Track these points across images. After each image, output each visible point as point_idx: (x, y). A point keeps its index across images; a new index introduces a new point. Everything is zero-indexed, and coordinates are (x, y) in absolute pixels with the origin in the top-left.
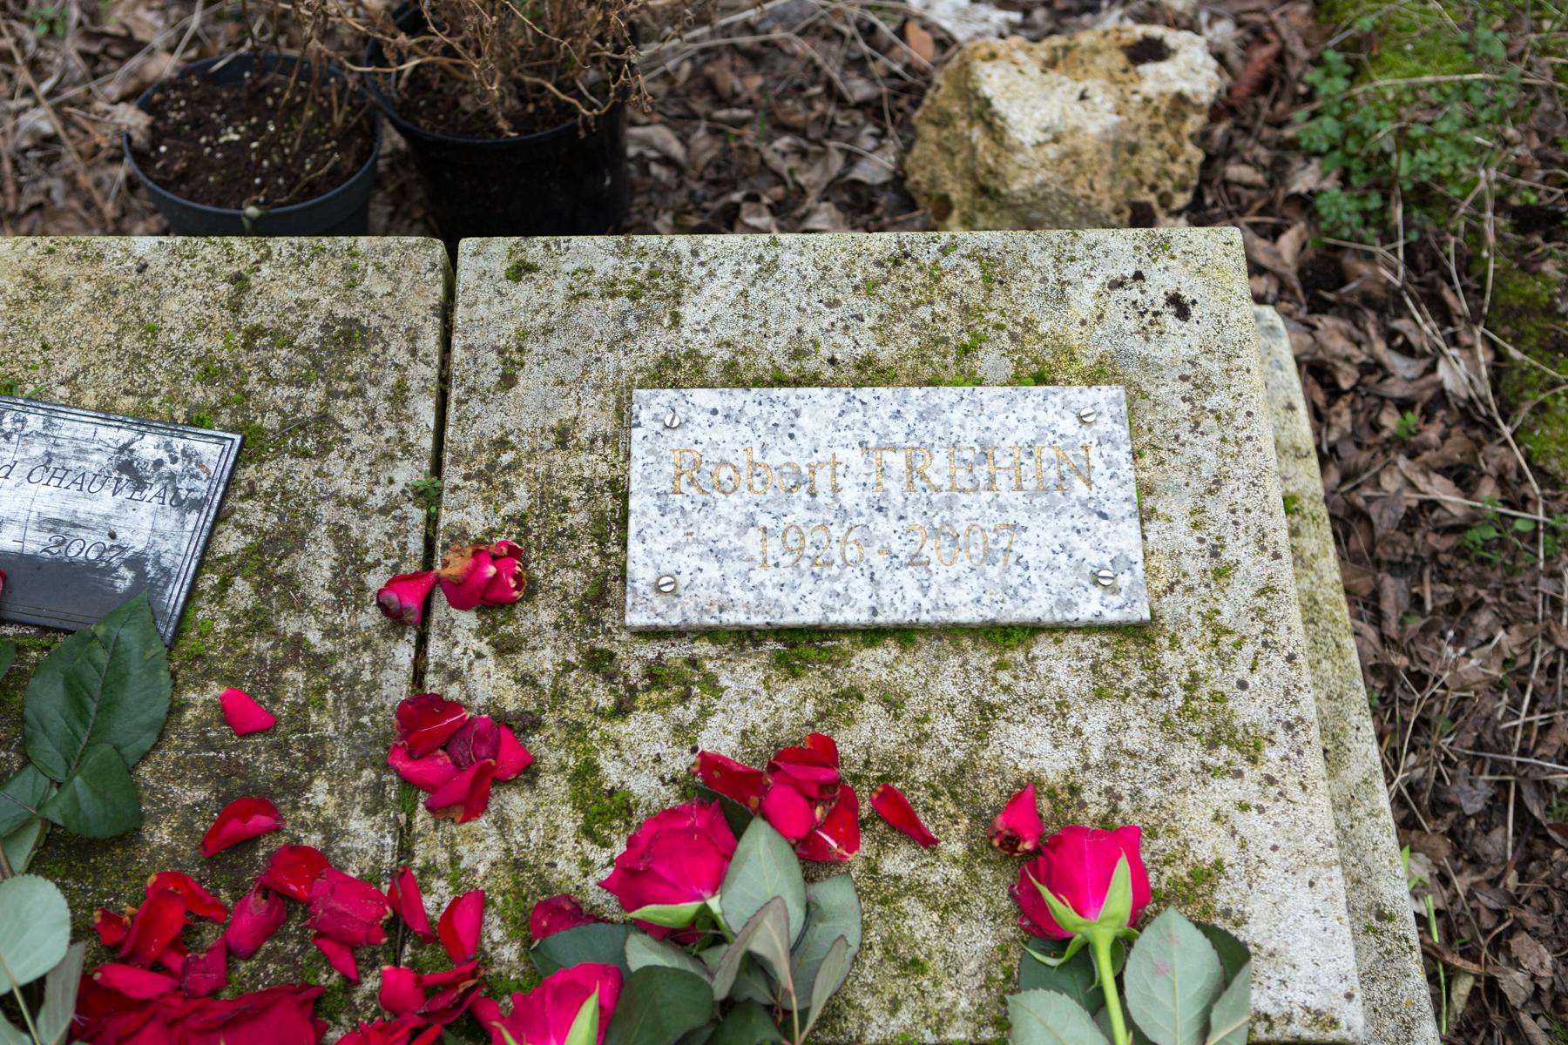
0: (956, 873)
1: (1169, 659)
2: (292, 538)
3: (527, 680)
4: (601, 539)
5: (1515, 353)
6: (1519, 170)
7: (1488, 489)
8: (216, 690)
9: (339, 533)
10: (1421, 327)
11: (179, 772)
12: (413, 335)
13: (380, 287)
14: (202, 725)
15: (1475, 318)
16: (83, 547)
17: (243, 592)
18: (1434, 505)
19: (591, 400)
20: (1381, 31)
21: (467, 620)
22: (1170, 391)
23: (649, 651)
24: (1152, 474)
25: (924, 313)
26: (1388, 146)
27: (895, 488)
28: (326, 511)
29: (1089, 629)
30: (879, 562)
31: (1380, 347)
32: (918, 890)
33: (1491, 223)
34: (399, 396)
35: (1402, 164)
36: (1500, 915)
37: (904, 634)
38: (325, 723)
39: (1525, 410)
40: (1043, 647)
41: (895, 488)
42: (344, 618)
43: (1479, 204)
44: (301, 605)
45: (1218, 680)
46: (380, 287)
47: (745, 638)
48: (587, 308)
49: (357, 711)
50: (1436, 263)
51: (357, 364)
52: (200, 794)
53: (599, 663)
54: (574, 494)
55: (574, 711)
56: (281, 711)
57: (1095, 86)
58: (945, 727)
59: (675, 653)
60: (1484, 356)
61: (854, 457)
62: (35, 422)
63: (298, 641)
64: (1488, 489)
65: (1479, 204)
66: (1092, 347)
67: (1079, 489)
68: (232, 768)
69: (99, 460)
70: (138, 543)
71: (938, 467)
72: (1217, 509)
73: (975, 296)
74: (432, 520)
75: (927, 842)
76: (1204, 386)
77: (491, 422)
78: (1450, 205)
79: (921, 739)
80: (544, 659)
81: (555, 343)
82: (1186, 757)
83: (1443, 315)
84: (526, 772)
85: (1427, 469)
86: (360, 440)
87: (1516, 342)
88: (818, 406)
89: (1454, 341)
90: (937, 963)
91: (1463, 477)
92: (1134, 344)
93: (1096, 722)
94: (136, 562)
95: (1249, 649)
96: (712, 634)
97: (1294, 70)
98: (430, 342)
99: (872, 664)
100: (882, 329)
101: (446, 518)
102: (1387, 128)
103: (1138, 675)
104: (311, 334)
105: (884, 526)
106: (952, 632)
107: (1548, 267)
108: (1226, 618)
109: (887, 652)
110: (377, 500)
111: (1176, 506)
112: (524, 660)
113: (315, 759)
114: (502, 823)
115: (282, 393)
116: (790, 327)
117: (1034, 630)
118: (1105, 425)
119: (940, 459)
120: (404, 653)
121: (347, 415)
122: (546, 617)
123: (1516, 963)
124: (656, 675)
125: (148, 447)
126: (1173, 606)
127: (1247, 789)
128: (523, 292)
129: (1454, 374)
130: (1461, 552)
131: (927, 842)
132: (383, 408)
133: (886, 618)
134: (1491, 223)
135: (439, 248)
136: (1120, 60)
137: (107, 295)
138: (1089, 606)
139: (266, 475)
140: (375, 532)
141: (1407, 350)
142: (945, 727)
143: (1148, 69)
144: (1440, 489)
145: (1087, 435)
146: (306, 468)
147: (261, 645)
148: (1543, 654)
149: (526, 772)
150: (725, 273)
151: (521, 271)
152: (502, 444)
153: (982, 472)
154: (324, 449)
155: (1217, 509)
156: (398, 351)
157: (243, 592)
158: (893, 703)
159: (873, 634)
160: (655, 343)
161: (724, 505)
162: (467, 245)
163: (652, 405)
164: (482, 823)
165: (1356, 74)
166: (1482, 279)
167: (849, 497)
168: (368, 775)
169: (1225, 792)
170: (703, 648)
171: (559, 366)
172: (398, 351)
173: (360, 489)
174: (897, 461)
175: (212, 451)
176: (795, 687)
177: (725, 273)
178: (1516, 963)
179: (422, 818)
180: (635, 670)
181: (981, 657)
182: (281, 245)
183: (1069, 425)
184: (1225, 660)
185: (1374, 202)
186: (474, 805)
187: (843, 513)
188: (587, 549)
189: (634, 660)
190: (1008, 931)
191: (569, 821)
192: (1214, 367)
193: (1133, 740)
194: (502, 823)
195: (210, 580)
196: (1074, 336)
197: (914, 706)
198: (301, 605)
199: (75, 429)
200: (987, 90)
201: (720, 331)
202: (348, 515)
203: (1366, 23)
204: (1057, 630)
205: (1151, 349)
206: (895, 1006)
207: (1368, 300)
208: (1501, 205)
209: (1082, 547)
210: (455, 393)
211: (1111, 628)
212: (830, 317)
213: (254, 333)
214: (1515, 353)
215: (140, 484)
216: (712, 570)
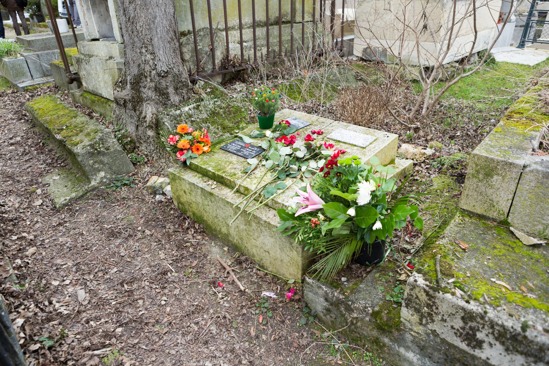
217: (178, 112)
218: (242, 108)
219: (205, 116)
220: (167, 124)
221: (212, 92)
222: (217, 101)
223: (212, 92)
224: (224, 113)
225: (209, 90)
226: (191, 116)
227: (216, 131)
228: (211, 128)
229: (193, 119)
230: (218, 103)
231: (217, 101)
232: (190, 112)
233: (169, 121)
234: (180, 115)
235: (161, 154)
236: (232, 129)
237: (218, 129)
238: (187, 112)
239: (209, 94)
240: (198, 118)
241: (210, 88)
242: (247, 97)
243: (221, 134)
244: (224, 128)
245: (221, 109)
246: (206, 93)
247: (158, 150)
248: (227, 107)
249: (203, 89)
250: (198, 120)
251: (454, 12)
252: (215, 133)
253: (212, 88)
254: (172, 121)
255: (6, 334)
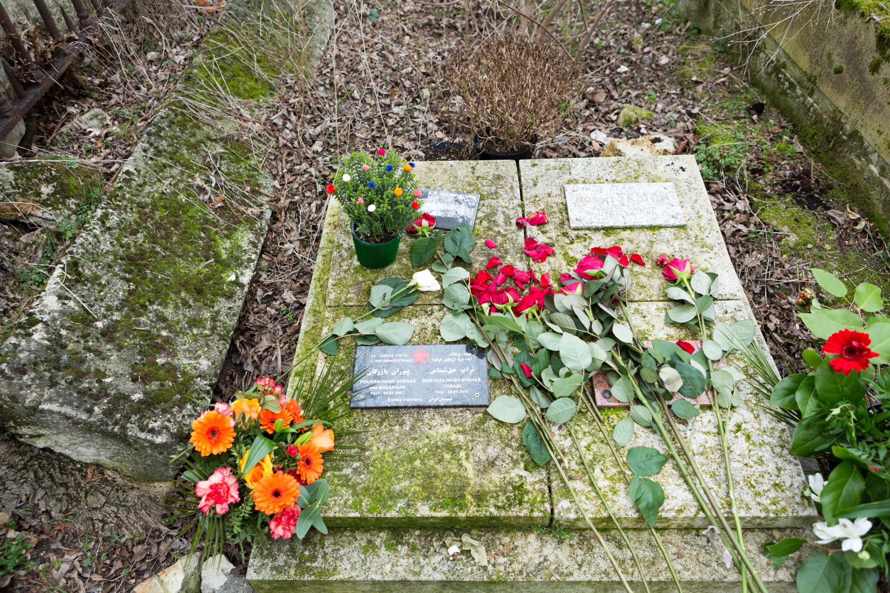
0: (650, 271)
1: (690, 232)
2: (494, 214)
3: (550, 238)
4: (561, 213)
5: (755, 199)
6: (751, 161)
7: (752, 226)
8: (483, 241)
9: (504, 213)
10: (732, 197)
11: (478, 254)
12: (513, 177)
13: (504, 169)
14: (481, 247)
15: (744, 193)
16: (451, 215)
17: (485, 223)
18: (739, 230)
19: (554, 188)
20: (712, 136)
21: (535, 228)
22: (683, 185)
23: (576, 232)
24: (682, 199)
25: (626, 171)
26: (718, 158)
27: (626, 202)
28: (500, 209)
29: (672, 227)
30: (625, 215)
31: (722, 200)
32: (642, 274)
33: (746, 173)
34: (512, 188)
35: (722, 162)
36: (765, 312)
37: (631, 228)
38: (507, 246)
39: (759, 211)
40: (662, 230)
41: (626, 202)
42: (508, 228)
43: (742, 169)
44: (498, 226)
45: (701, 236)
46: (504, 169)
47: (597, 229)
48: (550, 172)
49: (513, 244)
50: (733, 181)
51: (502, 182)
52: (483, 259)
53: (565, 235)
54: (554, 205)
55: (561, 243)
56: (498, 244)
57: (645, 148)
58: (643, 245)
59: (581, 233)
60: (748, 202)
61: (616, 196)
62: (436, 193)
63: (499, 232)
64: (752, 226)
65: (742, 169)
66: (665, 176)
67: (666, 201)
68: (489, 254)
69: (450, 200)
70: (462, 214)
71: (635, 197)
72: (697, 206)
73: (637, 168)
74: (523, 211)
75: (643, 264)
76: (691, 183)
77: (533, 192)
78: (735, 170)
79: (638, 247)
80: (553, 234)
81: (544, 178)
82: (697, 249)
83: (737, 193)
84: (553, 254)
85: (737, 222)
86: (505, 196)
87: (755, 197)
88: (606, 187)
89: (739, 198)
90: (648, 286)
91: (746, 224)
92: (674, 176)
93: (677, 244)
94: (462, 217)
95: (708, 231)
96: (589, 229)
97: (691, 147)
98: (517, 178)
99: (625, 234)
100: (617, 174)
101: (526, 210)
102: (718, 154)
103: (684, 235)
104: (490, 177)
105: (625, 208)
106: (642, 228)
107: (761, 181)
108: (702, 225)
109: (628, 232)
110: (511, 206)
111: (688, 205)
112: (548, 235)
113: (507, 252)
114: (549, 263)
115: (486, 188)
116: (596, 174)
117: (660, 227)
118: (670, 189)
119: (635, 196)
120: (522, 233)
121: (501, 191)
122: (552, 227)
123: (771, 321)
124: (578, 237)
125: (460, 197)
126: (689, 223)
127: (712, 254)
128: (535, 169)
129: (740, 206)
130: (748, 241)
131: (643, 264)
132: (509, 191)
133: (628, 224)
134: (746, 173)
135: (514, 162)
136: (650, 143)
137: (445, 171)
138: (672, 222)
139: (486, 202)
140: (511, 213)
141: (729, 201)
142: (643, 245)
143: (657, 144)
144: (741, 227)
145: (666, 191)
146: (494, 201)
147: (490, 233)
148: (770, 259)
149: (553, 254)
150: (580, 165)
151: (534, 165)
152: (536, 196)
153: (644, 198)
154: (498, 198)
155: (697, 206)
156: (510, 180)
157: (485, 223)
158: (631, 241)
159: (625, 228)
160: (567, 177)
161: (588, 205)
162: (521, 161)
163: (569, 188)
164: (545, 263)
165: (707, 145)
166: (745, 185)
167: (616, 203)
168: (519, 255)
169: (706, 256)
170: (587, 232)
171: (546, 182)
172: (510, 180)
173: (507, 205)
174: (625, 197)
175: (475, 198)
176: (609, 239)
177: (580, 165)
178: (771, 321)
179: (532, 262)
180: (573, 236)
181: (649, 233)
182: (481, 162)
183: (663, 189)
184: (703, 232)
185: (716, 171)
186: (543, 260)
187: (615, 206)
188: (558, 215)
189: (573, 234)
190: (663, 280)
191: (564, 263)
192: (693, 180)
193: (685, 247)
194: (549, 263)
195: (478, 221)
196: (660, 175)
197: (636, 242)
198: (498, 226)
199: (444, 194)
200: (619, 148)
201: (580, 175)
202: (505, 209)
203: (709, 135)
204: (665, 227)
205: (677, 177)
206: (640, 294)
207: (717, 192)
208: (747, 169)
209: (669, 211)
210: (524, 188)
211: (677, 227)
212: (605, 172)
213: (478, 178)
214: (755, 199)
215: (460, 203)
216: (588, 216)
217: (39, 335)
218: (175, 194)
219: (120, 289)
220: (55, 407)
221: (63, 192)
222: (106, 216)
223: (63, 192)
224: (153, 240)
225: (46, 190)
226: (85, 319)
227: (190, 313)
228: (169, 312)
229: (100, 324)
230: (113, 220)
231: (106, 216)
232: (71, 304)
233: (48, 393)
234: (57, 343)
235: (65, 485)
236: (214, 277)
237: (185, 304)
238: (62, 313)
239: (57, 201)
240: (109, 308)
241: (48, 181)
242: (159, 152)
243: (207, 315)
244: (200, 292)
245: (134, 233)
246: (44, 203)
247: (47, 482)
248: (144, 217)
249: (23, 195)
250: (116, 316)
251: (521, 186)
252: (194, 322)
253: (54, 179)
254: (53, 384)
255: (820, 542)
